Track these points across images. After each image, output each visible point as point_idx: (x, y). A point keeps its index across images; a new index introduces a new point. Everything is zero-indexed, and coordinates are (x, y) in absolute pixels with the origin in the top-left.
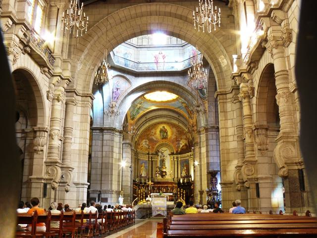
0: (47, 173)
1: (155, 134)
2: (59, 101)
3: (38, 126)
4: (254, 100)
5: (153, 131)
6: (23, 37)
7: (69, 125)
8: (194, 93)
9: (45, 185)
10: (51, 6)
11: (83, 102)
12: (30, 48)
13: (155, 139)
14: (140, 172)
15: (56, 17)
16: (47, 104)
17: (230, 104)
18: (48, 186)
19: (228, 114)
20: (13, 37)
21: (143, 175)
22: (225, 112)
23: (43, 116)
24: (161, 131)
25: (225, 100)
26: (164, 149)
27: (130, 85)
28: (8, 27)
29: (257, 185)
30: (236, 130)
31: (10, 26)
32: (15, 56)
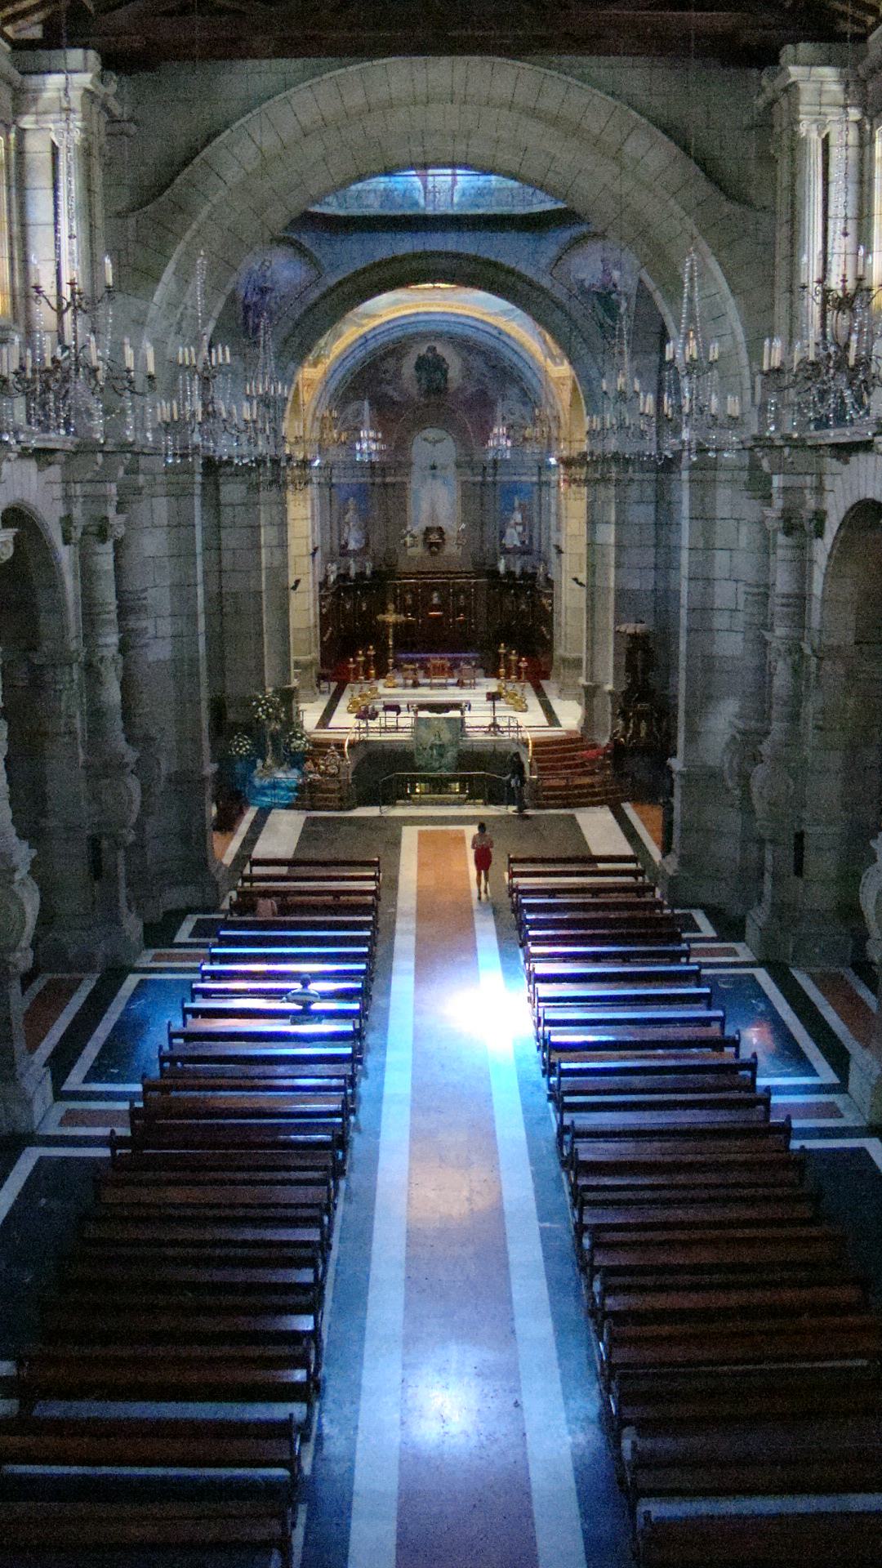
0: (95, 797)
1: (397, 374)
2: (103, 541)
3: (47, 646)
4: (822, 549)
5: (390, 363)
7: (134, 583)
8: (577, 308)
9: (94, 843)
11: (174, 478)
13: (396, 397)
14: (340, 536)
15: (49, 183)
16: (66, 556)
17: (729, 492)
18: (105, 844)
19: (719, 527)
21: (352, 546)
22: (704, 517)
23: (59, 608)
24: (422, 363)
25: (710, 474)
26: (431, 433)
27: (314, 272)
29: (800, 837)
30: (742, 598)
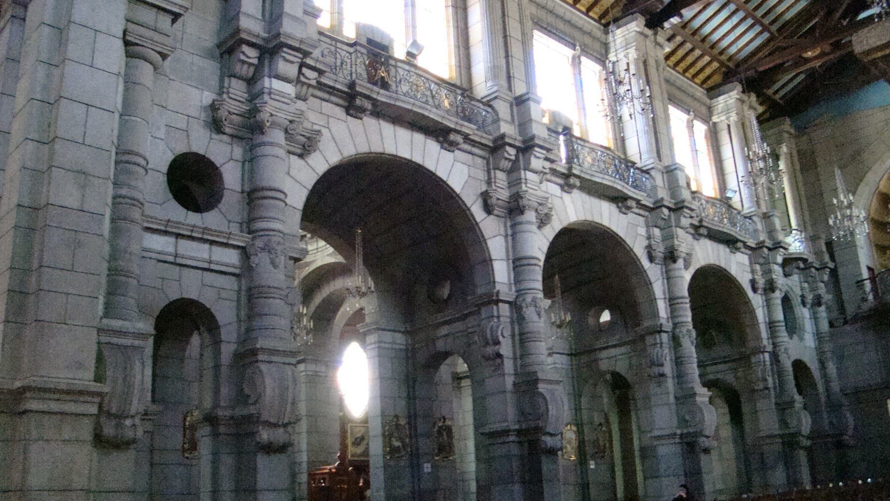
3: (752, 344)
6: (547, 165)
10: (715, 124)
12: (706, 227)
20: (523, 176)
28: (665, 219)
31: (666, 218)
32: (536, 210)
